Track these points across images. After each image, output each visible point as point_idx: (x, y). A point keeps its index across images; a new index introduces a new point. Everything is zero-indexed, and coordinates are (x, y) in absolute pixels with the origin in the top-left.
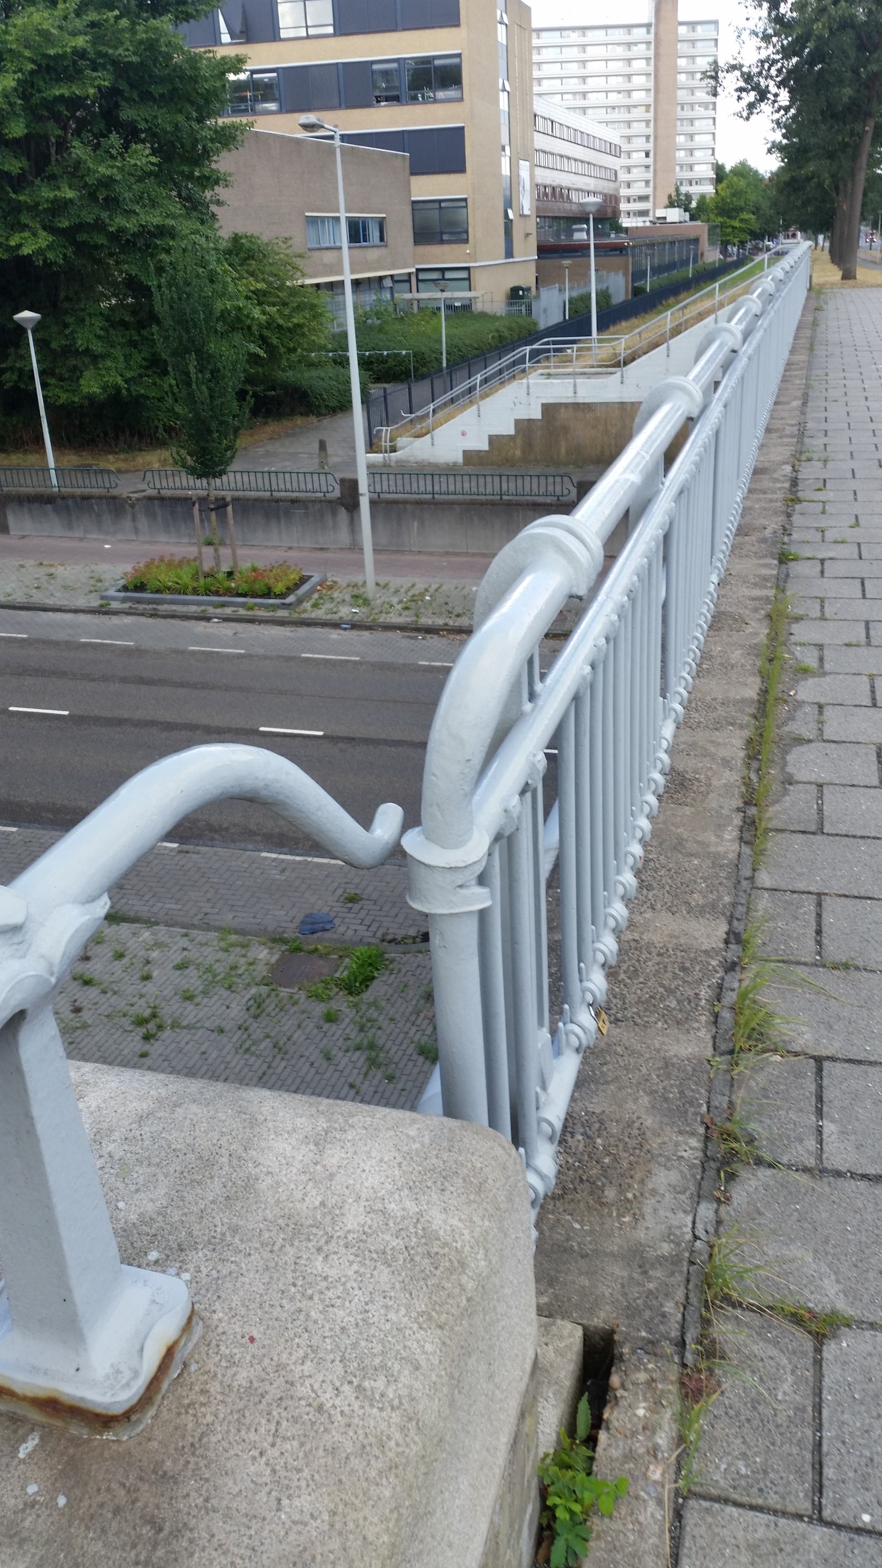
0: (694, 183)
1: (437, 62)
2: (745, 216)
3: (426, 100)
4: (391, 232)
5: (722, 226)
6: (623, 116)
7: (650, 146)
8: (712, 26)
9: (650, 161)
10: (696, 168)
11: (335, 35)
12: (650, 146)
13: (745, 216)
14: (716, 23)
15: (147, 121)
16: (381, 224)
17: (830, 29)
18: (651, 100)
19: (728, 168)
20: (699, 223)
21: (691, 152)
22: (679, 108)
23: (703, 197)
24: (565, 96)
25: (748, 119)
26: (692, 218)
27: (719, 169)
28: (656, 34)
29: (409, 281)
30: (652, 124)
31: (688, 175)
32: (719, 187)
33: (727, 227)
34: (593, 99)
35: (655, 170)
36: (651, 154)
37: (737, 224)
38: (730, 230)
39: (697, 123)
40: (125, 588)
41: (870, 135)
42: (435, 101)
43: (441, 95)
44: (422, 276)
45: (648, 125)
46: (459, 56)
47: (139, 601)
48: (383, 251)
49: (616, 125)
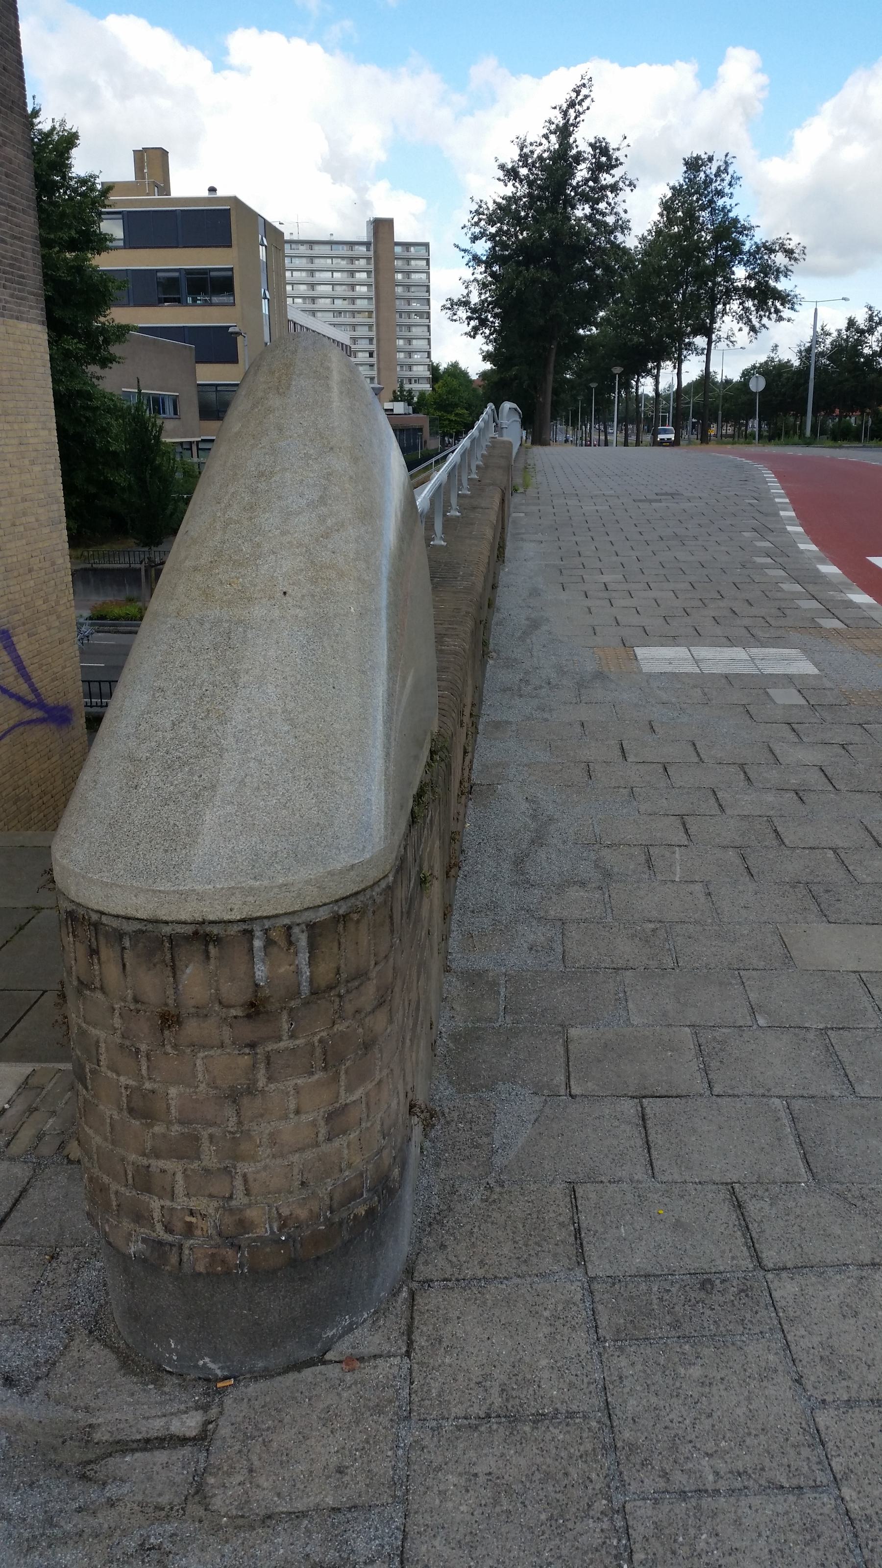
0: (413, 381)
1: (213, 274)
2: (459, 411)
3: (207, 304)
4: (182, 407)
5: (441, 418)
6: (348, 320)
7: (373, 347)
8: (424, 248)
9: (374, 360)
10: (415, 368)
11: (125, 247)
12: (373, 347)
13: (459, 411)
14: (426, 245)
15: (70, 319)
16: (175, 401)
17: (525, 284)
18: (372, 307)
19: (442, 367)
20: (421, 415)
21: (410, 354)
22: (398, 316)
23: (422, 394)
24: (297, 300)
25: (474, 338)
26: (415, 411)
27: (434, 369)
28: (375, 252)
29: (191, 449)
30: (374, 328)
31: (408, 374)
32: (436, 386)
33: (445, 420)
34: (323, 303)
35: (379, 369)
36: (375, 355)
37: (453, 417)
38: (447, 422)
39: (414, 329)
40: (91, 618)
41: (554, 351)
42: (211, 305)
43: (215, 299)
44: (201, 446)
45: (370, 330)
46: (231, 269)
47: (104, 625)
48: (176, 422)
49: (343, 327)
